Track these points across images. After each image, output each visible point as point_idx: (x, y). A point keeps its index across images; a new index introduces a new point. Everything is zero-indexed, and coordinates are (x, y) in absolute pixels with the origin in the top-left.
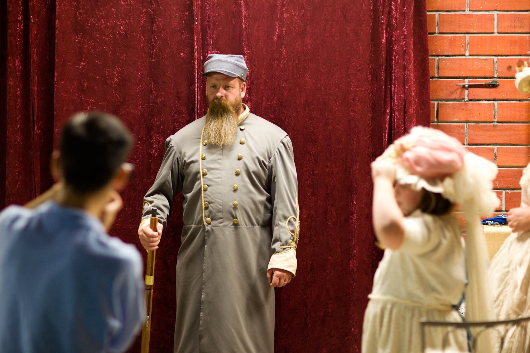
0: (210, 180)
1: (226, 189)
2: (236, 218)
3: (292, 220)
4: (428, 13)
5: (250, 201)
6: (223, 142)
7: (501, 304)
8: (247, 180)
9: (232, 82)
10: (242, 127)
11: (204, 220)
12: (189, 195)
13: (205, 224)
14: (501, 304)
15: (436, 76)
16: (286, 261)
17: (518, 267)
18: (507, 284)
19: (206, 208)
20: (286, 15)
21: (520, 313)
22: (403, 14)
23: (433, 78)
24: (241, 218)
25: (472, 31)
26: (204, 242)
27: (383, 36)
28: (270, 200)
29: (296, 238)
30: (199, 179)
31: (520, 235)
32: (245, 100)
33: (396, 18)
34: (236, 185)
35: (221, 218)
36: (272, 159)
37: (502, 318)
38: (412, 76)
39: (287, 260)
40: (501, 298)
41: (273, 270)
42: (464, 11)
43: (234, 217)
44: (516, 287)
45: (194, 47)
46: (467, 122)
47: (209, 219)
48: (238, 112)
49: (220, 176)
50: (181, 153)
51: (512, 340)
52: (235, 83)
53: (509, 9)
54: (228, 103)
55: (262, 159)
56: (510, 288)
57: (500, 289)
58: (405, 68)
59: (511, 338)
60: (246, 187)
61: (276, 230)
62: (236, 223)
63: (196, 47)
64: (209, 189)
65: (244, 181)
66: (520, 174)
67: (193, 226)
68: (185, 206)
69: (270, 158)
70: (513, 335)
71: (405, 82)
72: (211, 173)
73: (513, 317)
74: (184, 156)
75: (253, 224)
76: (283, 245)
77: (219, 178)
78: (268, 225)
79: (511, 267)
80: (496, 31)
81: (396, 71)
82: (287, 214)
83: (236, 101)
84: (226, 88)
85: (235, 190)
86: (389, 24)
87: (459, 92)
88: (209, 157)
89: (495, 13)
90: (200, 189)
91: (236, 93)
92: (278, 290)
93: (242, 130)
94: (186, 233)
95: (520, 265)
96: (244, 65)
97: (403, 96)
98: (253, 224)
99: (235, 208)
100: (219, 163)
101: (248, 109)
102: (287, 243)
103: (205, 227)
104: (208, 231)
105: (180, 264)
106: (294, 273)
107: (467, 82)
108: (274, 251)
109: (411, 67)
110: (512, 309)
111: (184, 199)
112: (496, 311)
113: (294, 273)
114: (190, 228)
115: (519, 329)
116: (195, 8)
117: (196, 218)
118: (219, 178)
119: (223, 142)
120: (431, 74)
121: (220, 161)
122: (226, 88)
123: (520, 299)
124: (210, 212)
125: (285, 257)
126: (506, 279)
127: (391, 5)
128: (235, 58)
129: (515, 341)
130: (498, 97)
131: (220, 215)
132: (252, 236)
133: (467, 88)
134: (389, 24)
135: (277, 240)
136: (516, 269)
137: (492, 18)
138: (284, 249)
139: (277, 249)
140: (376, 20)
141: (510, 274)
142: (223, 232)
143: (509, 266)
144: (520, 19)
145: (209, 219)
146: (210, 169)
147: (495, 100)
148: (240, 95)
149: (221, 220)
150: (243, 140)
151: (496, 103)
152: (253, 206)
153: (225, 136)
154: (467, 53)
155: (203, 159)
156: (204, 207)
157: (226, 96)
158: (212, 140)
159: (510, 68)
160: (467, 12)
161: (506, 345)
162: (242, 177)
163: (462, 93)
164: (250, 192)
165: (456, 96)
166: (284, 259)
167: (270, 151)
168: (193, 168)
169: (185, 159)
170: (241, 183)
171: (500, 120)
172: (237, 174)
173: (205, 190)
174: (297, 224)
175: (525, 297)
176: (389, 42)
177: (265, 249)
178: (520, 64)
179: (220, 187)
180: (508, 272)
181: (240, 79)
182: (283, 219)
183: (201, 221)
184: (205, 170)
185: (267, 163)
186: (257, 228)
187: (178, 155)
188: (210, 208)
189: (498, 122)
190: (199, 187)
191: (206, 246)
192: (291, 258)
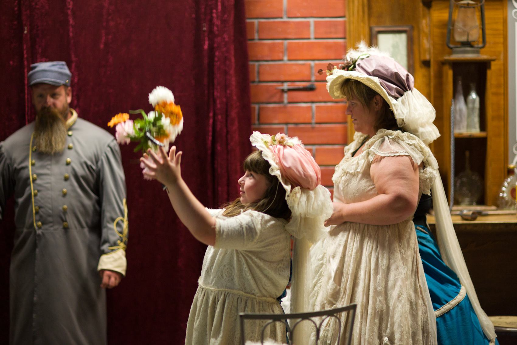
0: (40, 185)
1: (55, 194)
2: (66, 221)
3: (120, 222)
4: (248, 21)
5: (79, 204)
6: (54, 151)
7: (316, 294)
8: (76, 184)
9: (58, 90)
10: (70, 133)
11: (35, 224)
12: (21, 200)
13: (36, 227)
14: (316, 294)
15: (257, 80)
16: (114, 261)
17: (331, 259)
18: (321, 275)
19: (37, 213)
20: (112, 24)
21: (334, 302)
22: (224, 22)
23: (254, 82)
24: (71, 221)
25: (289, 36)
26: (35, 246)
27: (204, 44)
28: (99, 202)
29: (125, 239)
30: (29, 185)
31: (333, 229)
32: (71, 105)
33: (217, 26)
34: (65, 190)
35: (51, 222)
36: (100, 163)
37: (317, 309)
38: (233, 81)
39: (116, 260)
40: (316, 288)
41: (103, 271)
42: (281, 18)
43: (63, 221)
44: (329, 278)
45: (23, 55)
46: (287, 124)
47: (40, 223)
48: (66, 118)
49: (49, 181)
50: (11, 159)
51: (328, 328)
52: (62, 91)
53: (324, 15)
54: (56, 110)
55: (89, 163)
56: (324, 279)
57: (315, 281)
58: (226, 73)
59: (326, 326)
60: (74, 191)
61: (104, 231)
62: (66, 226)
63: (25, 56)
64: (39, 194)
65: (72, 185)
66: (333, 172)
67: (25, 230)
68: (17, 210)
69: (97, 162)
70: (328, 324)
71: (226, 87)
72: (41, 179)
73: (328, 308)
74: (14, 162)
75: (82, 227)
76: (111, 246)
77: (48, 183)
78: (97, 227)
79: (325, 259)
80: (312, 36)
81: (218, 76)
82: (114, 216)
83: (64, 107)
84: (54, 96)
85: (64, 195)
86: (211, 31)
87: (278, 95)
88: (38, 164)
89: (312, 20)
90: (30, 194)
91: (64, 99)
92: (110, 291)
93: (70, 136)
94: (18, 236)
95: (334, 257)
96: (67, 71)
97: (224, 100)
98: (82, 227)
99: (65, 212)
100: (48, 169)
101: (75, 115)
102: (115, 244)
103: (35, 232)
104: (39, 235)
105: (12, 267)
106: (124, 273)
107: (286, 86)
108: (103, 253)
109: (232, 72)
110: (326, 299)
111: (16, 203)
112: (311, 301)
113: (124, 273)
114: (22, 232)
115: (333, 318)
116: (24, 18)
117: (28, 222)
118: (48, 183)
119: (54, 151)
120: (251, 78)
121: (49, 167)
122: (54, 96)
123: (334, 289)
124: (41, 217)
125: (113, 257)
126: (320, 271)
127: (212, 13)
128: (58, 66)
129: (330, 329)
130: (315, 99)
131: (50, 219)
132: (81, 237)
133: (286, 92)
134: (211, 31)
135: (106, 241)
136: (329, 262)
137: (308, 24)
138: (112, 250)
139: (106, 250)
140: (198, 28)
141: (324, 266)
142: (53, 234)
143: (322, 258)
144: (335, 24)
145: (40, 223)
146: (39, 175)
147: (313, 102)
148: (66, 101)
149: (51, 224)
150: (71, 145)
151: (314, 106)
152: (82, 209)
153: (55, 144)
154: (286, 58)
155: (33, 165)
156: (34, 211)
157: (54, 105)
158: (43, 148)
159: (320, 71)
160: (285, 19)
161: (321, 333)
162: (71, 181)
163: (282, 97)
164: (78, 195)
165: (276, 99)
166: (112, 259)
167: (98, 154)
168: (23, 174)
169: (15, 165)
170: (70, 188)
171: (318, 121)
172: (66, 179)
173: (35, 195)
174: (125, 225)
175: (338, 287)
176: (212, 49)
177: (95, 249)
178: (330, 68)
179: (50, 192)
180: (322, 264)
181: (65, 86)
182: (110, 221)
183: (32, 225)
184: (35, 176)
185: (94, 167)
186: (86, 230)
187: (8, 161)
188: (41, 213)
189: (317, 123)
190: (29, 192)
191: (37, 250)
192: (120, 258)
